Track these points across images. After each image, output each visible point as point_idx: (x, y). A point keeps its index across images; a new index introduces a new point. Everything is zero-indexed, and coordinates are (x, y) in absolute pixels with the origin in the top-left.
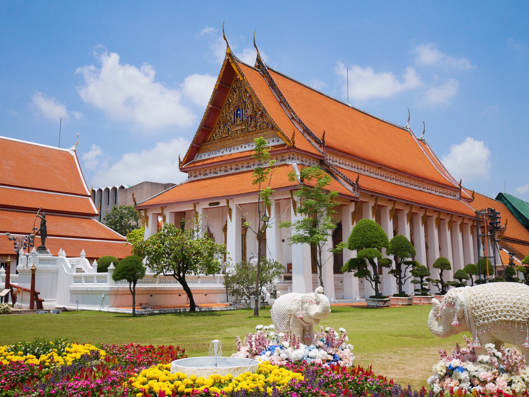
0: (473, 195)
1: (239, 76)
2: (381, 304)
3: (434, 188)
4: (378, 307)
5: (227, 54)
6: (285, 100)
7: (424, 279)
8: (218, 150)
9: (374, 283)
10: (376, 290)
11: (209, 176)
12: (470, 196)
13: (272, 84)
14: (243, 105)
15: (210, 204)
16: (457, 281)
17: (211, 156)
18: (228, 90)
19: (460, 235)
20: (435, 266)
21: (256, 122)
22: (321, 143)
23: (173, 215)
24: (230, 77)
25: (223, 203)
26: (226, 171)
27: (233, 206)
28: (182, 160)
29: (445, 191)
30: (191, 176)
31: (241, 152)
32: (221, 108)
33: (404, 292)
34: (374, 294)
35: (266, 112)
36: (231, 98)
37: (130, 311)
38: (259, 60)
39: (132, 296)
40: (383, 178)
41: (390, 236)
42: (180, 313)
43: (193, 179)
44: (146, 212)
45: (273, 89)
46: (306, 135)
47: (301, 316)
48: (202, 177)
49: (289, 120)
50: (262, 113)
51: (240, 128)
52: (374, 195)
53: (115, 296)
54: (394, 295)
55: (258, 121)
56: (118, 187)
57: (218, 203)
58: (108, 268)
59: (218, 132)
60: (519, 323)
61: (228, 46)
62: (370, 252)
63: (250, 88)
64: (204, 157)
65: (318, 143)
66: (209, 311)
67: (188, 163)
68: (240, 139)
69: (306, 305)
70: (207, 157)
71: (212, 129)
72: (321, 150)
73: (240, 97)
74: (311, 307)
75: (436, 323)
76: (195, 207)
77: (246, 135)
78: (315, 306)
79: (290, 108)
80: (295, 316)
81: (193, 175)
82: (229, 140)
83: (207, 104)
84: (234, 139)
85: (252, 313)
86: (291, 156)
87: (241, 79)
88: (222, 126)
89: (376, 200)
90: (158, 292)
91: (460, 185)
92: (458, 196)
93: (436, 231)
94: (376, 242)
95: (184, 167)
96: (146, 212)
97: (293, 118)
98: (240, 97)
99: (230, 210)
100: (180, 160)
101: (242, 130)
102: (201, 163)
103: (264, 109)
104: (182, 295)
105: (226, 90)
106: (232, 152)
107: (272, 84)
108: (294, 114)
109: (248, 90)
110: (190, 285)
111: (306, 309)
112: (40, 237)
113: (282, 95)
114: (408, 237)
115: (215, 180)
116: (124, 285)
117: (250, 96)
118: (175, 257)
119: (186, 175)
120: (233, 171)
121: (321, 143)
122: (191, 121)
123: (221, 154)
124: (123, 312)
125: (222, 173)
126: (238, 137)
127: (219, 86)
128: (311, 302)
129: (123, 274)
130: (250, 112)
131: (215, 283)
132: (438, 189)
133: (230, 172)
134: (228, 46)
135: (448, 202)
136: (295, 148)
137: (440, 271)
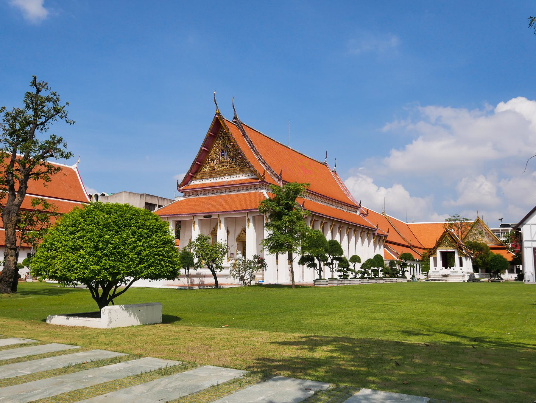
0: (367, 212)
3: (344, 207)
5: (216, 113)
9: (318, 271)
12: (365, 212)
13: (244, 135)
15: (205, 217)
24: (218, 128)
28: (179, 184)
29: (351, 209)
56: (99, 194)
57: (210, 216)
61: (217, 109)
63: (234, 139)
91: (360, 205)
112: (4, 230)
117: (234, 145)
132: (346, 207)
134: (217, 109)
135: (342, 213)
136: (265, 182)
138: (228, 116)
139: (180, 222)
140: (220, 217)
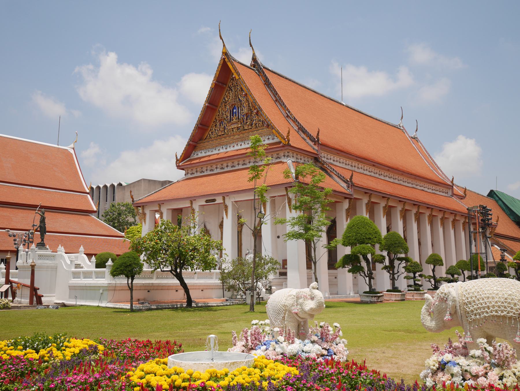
0: (465, 192)
1: (235, 75)
2: (375, 299)
3: (427, 185)
4: (371, 302)
5: (223, 53)
6: (280, 99)
7: (417, 275)
8: (215, 147)
9: (367, 279)
10: (370, 285)
11: (205, 173)
12: (461, 193)
13: (267, 83)
14: (239, 104)
15: (207, 201)
16: (450, 276)
17: (208, 154)
18: (224, 88)
19: (452, 232)
20: (428, 262)
21: (252, 120)
22: (316, 141)
23: (170, 212)
24: (226, 75)
25: (219, 200)
26: (222, 168)
27: (229, 202)
28: (179, 158)
29: (438, 188)
30: (188, 173)
31: (237, 150)
32: (217, 106)
33: (397, 288)
34: (390, 288)
35: (262, 110)
36: (227, 96)
37: (128, 306)
38: (254, 59)
39: (130, 291)
40: (377, 176)
41: (384, 233)
42: (177, 308)
43: (189, 176)
44: (143, 209)
45: (268, 87)
46: (301, 132)
47: (296, 311)
48: (199, 174)
49: (284, 119)
50: (258, 111)
51: (236, 126)
52: (368, 192)
53: (113, 291)
54: (388, 291)
55: (253, 119)
56: (116, 184)
57: (214, 200)
58: (106, 264)
59: (215, 130)
60: (510, 318)
61: (224, 46)
62: (364, 248)
63: (246, 86)
64: (200, 155)
65: (312, 141)
66: (206, 306)
67: (185, 160)
68: (236, 137)
69: (301, 301)
70: (203, 154)
71: (209, 127)
72: (316, 147)
73: (236, 96)
74: (306, 302)
75: (429, 318)
76: (192, 203)
77: (242, 133)
78: (310, 301)
79: (285, 106)
80: (290, 312)
81: (190, 172)
82: (225, 138)
83: (204, 103)
84: (230, 137)
85: (248, 308)
86: (286, 154)
87: (237, 78)
88: (218, 124)
89: (370, 196)
90: (155, 288)
92: (450, 193)
93: (428, 228)
94: (370, 239)
95: (180, 164)
96: (143, 209)
97: (288, 116)
98: (236, 96)
99: (226, 207)
100: (177, 157)
101: (238, 128)
102: (198, 161)
103: (260, 107)
104: (179, 291)
105: (223, 89)
106: (228, 149)
107: (267, 83)
108: (289, 112)
109: (244, 88)
110: (186, 281)
111: (301, 305)
113: (277, 94)
114: (401, 233)
115: (212, 177)
116: (123, 281)
117: (246, 95)
118: (172, 253)
119: (183, 172)
120: (229, 169)
121: (316, 141)
122: (188, 120)
123: (217, 152)
124: (121, 307)
125: (219, 171)
126: (234, 135)
127: (216, 84)
128: (305, 298)
129: (121, 270)
130: (245, 111)
131: (212, 278)
132: (431, 186)
133: (226, 169)
134: (224, 46)
135: (440, 199)
136: (290, 146)
137: (432, 267)
138: (244, 58)
139: (180, 210)
140: (227, 199)
